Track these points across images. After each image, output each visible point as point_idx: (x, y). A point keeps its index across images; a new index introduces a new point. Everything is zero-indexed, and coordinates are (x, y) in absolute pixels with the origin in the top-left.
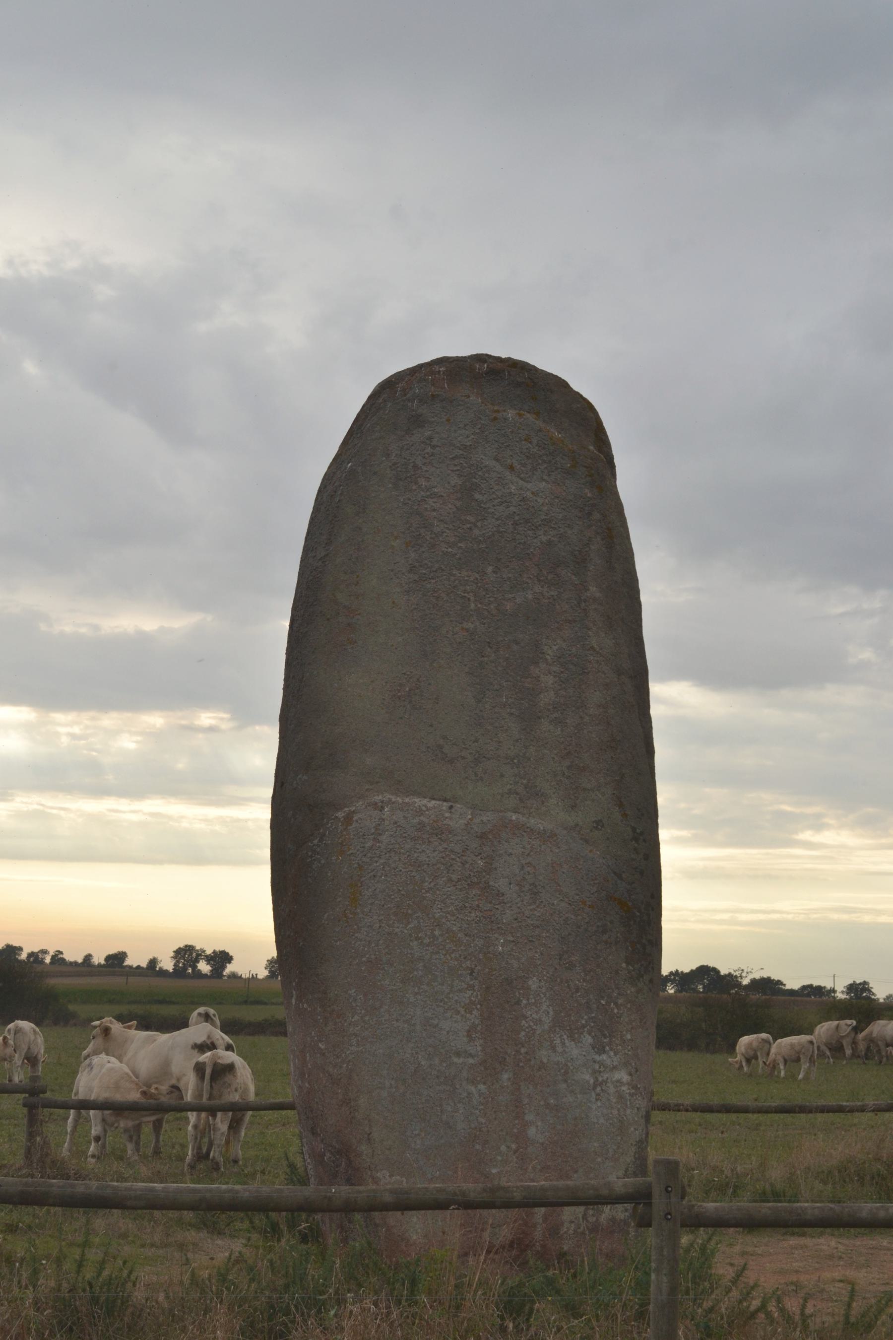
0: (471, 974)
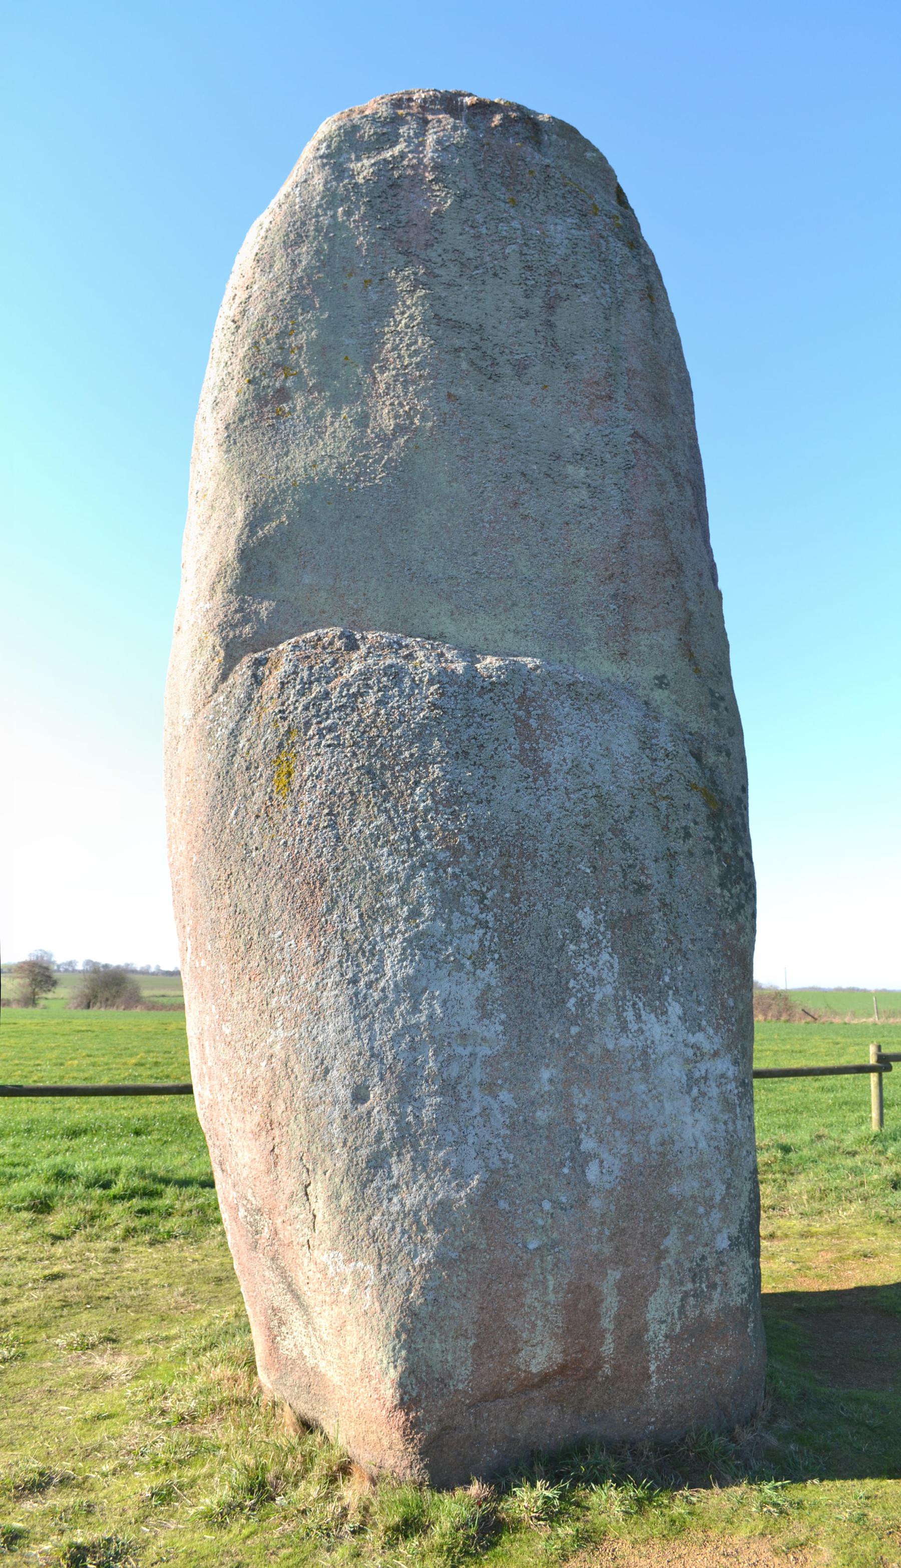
0: (481, 902)
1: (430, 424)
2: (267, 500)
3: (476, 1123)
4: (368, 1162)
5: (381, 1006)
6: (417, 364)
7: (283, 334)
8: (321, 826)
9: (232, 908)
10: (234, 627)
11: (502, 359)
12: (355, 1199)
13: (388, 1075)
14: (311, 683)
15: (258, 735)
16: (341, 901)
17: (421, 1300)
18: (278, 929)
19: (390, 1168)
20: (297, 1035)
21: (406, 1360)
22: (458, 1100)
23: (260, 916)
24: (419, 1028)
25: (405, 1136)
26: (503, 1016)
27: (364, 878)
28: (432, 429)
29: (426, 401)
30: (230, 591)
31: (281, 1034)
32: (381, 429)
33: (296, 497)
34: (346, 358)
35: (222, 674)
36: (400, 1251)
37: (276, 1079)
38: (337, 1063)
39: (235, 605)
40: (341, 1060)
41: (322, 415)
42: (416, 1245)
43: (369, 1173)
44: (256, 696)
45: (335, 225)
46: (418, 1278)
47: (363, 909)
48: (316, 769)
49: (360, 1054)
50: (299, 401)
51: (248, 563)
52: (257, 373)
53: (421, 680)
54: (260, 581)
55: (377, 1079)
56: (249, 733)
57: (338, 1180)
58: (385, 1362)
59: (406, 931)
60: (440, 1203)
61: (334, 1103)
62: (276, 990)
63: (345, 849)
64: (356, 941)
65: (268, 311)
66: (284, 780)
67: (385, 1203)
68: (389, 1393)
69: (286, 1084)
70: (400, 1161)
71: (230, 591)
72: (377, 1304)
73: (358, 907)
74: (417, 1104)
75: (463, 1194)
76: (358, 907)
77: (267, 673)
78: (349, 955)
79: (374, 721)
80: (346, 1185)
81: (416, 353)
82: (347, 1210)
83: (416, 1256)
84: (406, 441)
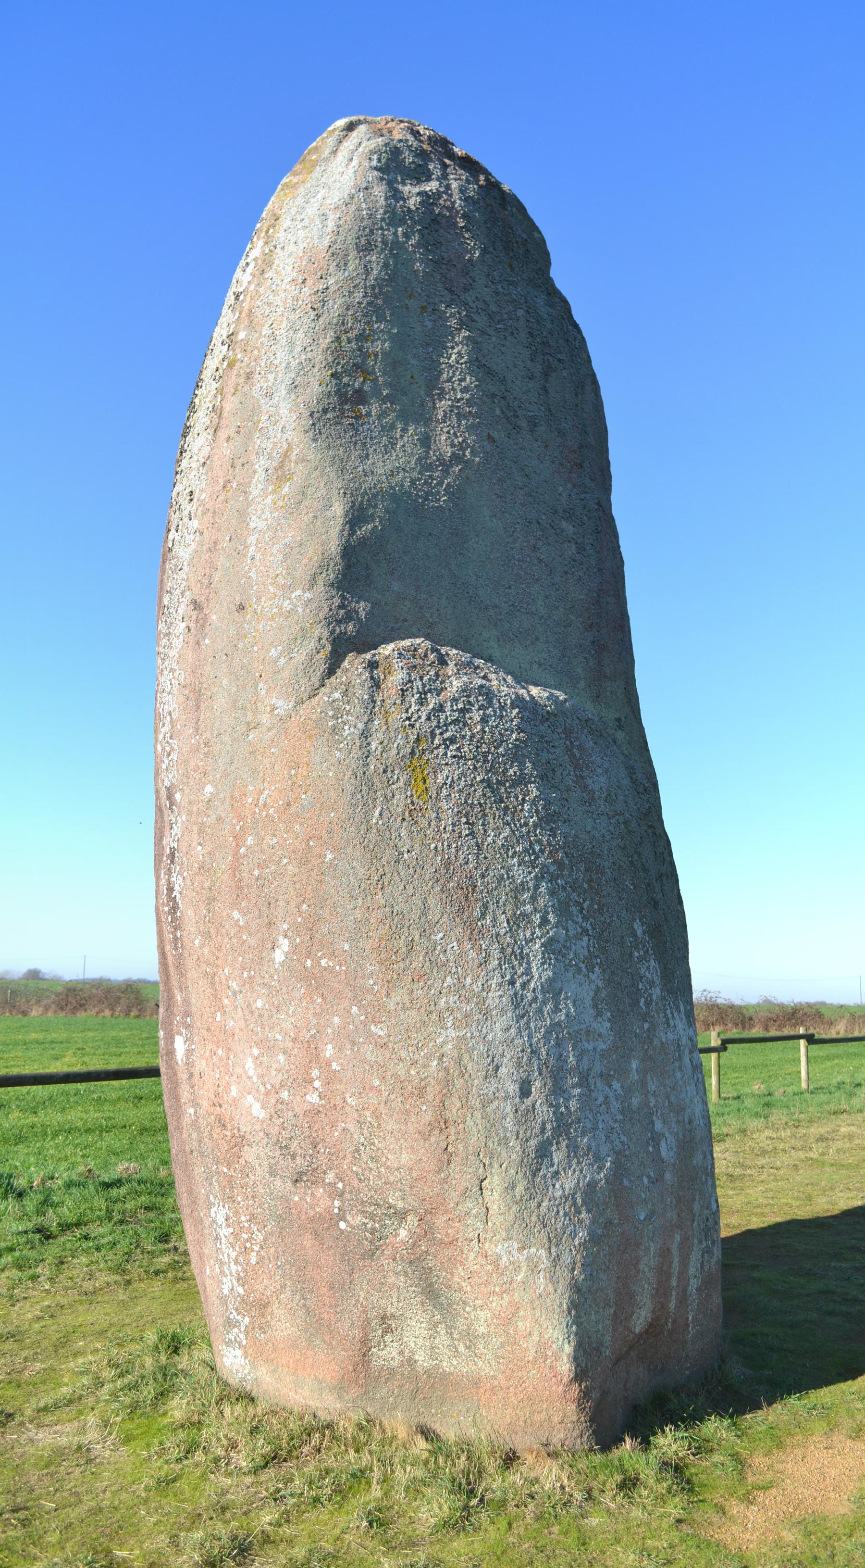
1: (477, 459)
2: (362, 501)
3: (601, 1111)
4: (536, 1152)
5: (533, 1005)
6: (467, 400)
7: (361, 338)
8: (464, 834)
9: (387, 909)
10: (339, 622)
11: (520, 413)
12: (528, 1188)
13: (544, 1070)
14: (425, 694)
15: (391, 739)
16: (491, 907)
17: (583, 1277)
18: (439, 932)
19: (552, 1156)
20: (469, 1035)
21: (576, 1334)
22: (590, 1090)
23: (420, 918)
24: (561, 1026)
25: (562, 1126)
26: (609, 1014)
27: (505, 886)
28: (479, 463)
29: (474, 438)
30: (332, 585)
31: (452, 1033)
32: (440, 454)
33: (385, 504)
34: (412, 377)
35: (329, 668)
36: (565, 1233)
37: (450, 1078)
38: (505, 1060)
39: (337, 601)
40: (509, 1057)
41: (393, 427)
42: (575, 1226)
43: (538, 1162)
44: (379, 699)
45: (396, 243)
46: (579, 1256)
47: (508, 915)
48: (447, 777)
49: (523, 1051)
50: (375, 409)
51: (349, 560)
52: (339, 369)
53: (506, 704)
54: (357, 580)
55: (536, 1074)
56: (380, 735)
57: (513, 1172)
58: (561, 1339)
59: (541, 937)
60: (589, 1185)
61: (506, 1098)
62: (444, 991)
63: (485, 858)
64: (508, 946)
65: (348, 309)
66: (422, 786)
67: (551, 1188)
68: (565, 1367)
69: (459, 1083)
70: (559, 1149)
71: (332, 585)
72: (550, 1285)
73: (504, 913)
74: (566, 1096)
75: (602, 1175)
76: (504, 913)
77: (382, 677)
78: (505, 957)
79: (483, 738)
80: (520, 1175)
81: (465, 390)
82: (521, 1200)
83: (575, 1236)
84: (460, 470)
